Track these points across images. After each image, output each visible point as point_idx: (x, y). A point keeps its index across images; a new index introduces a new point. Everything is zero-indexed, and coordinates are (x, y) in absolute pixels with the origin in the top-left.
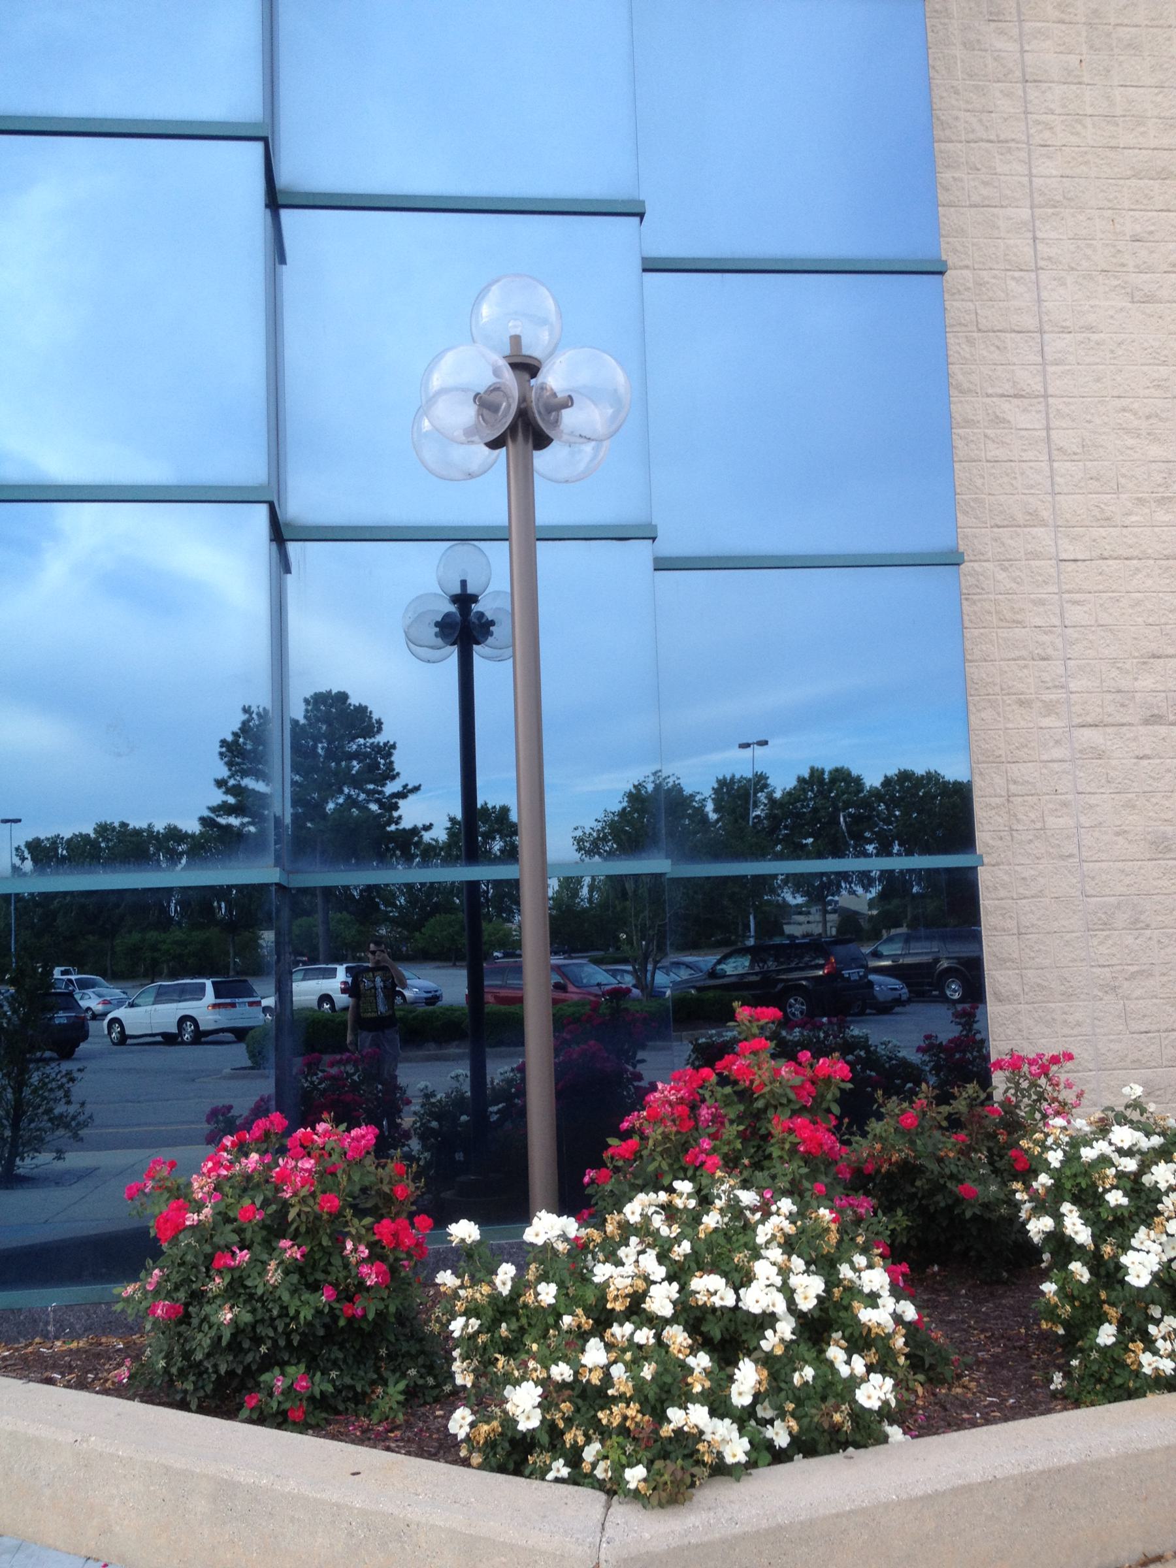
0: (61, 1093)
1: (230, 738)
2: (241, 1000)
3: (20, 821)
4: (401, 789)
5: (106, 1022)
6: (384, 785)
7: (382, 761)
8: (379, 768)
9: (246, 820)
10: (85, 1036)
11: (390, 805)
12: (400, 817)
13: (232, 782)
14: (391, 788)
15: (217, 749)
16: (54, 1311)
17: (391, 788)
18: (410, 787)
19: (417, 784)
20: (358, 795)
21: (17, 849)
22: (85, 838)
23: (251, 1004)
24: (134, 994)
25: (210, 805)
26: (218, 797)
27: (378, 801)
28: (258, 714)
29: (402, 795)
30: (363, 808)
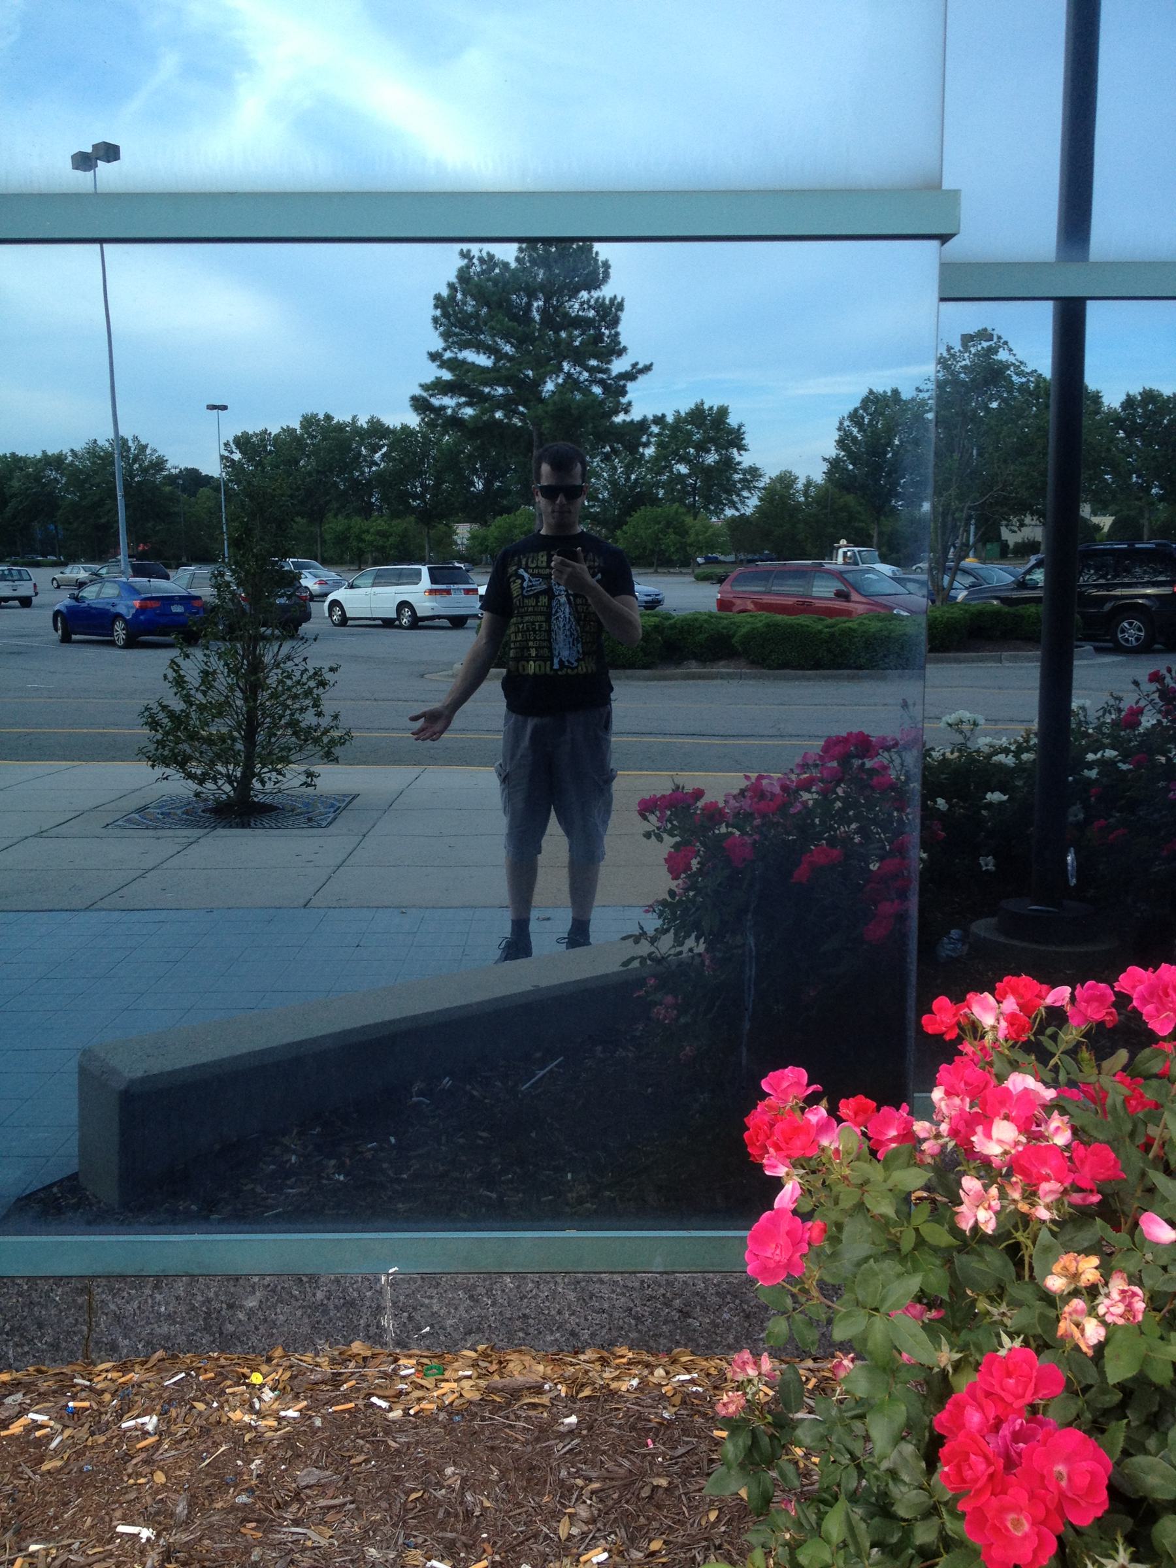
0: (308, 702)
1: (445, 292)
2: (456, 586)
3: (224, 408)
4: (629, 368)
5: (327, 604)
6: (609, 362)
7: (607, 332)
8: (602, 341)
9: (463, 399)
10: (307, 617)
11: (616, 389)
12: (629, 404)
13: (448, 355)
14: (618, 366)
15: (431, 312)
16: (393, 1284)
17: (618, 366)
18: (640, 366)
19: (648, 363)
20: (580, 373)
21: (226, 444)
22: (289, 431)
23: (467, 591)
24: (352, 577)
25: (422, 383)
26: (434, 373)
27: (601, 383)
28: (481, 259)
29: (630, 376)
30: (587, 392)
